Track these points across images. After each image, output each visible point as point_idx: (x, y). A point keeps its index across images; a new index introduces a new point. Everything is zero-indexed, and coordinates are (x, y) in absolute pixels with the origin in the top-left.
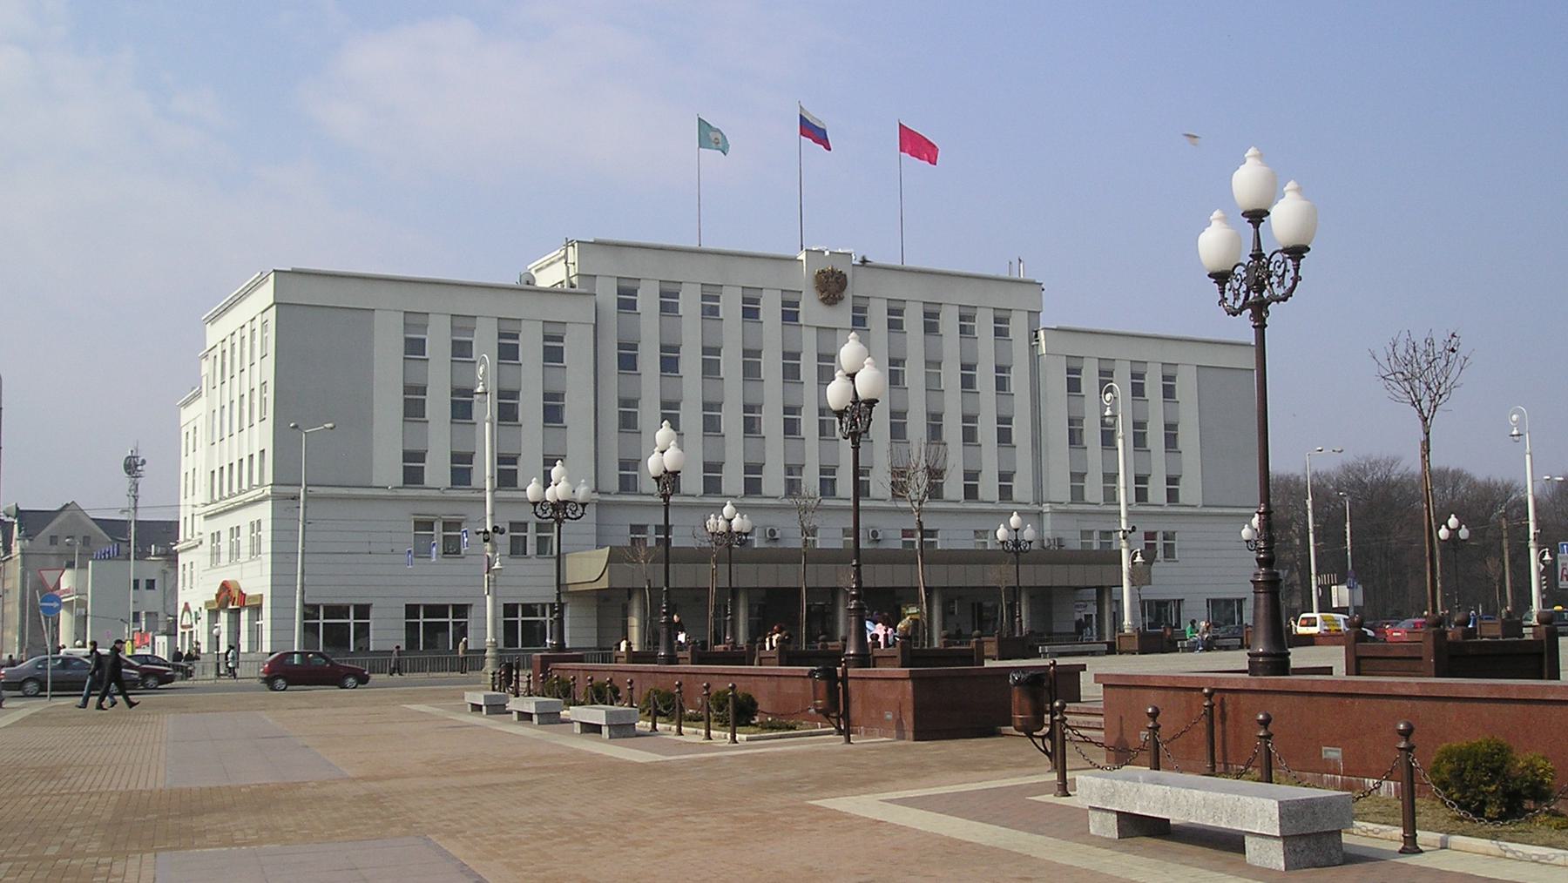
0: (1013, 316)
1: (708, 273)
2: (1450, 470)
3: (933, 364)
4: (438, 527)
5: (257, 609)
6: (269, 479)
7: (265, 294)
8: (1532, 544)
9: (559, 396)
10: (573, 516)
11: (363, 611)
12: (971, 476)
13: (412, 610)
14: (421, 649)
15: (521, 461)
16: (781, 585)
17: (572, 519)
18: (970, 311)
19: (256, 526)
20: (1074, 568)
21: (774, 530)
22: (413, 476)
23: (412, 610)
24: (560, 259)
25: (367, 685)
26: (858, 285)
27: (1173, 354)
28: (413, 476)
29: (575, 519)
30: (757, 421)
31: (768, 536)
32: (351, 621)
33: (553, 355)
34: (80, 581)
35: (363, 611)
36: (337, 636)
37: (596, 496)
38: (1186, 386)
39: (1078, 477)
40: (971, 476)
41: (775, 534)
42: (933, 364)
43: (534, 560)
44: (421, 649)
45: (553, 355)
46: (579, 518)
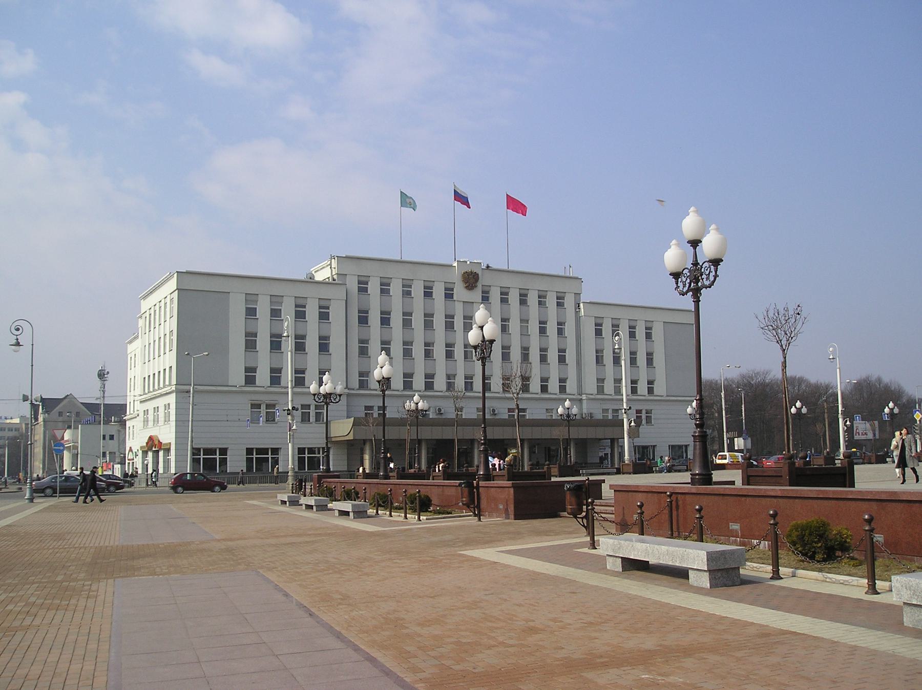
2: (797, 377)
3: (524, 321)
4: (263, 407)
5: (168, 450)
6: (174, 382)
7: (172, 284)
8: (840, 416)
9: (327, 338)
10: (335, 401)
13: (249, 451)
14: (254, 471)
17: (334, 403)
19: (167, 406)
22: (250, 380)
23: (249, 451)
24: (327, 266)
26: (484, 280)
27: (650, 316)
28: (250, 380)
29: (336, 403)
32: (218, 457)
33: (324, 316)
34: (75, 436)
37: (347, 391)
38: (658, 333)
40: (544, 380)
42: (524, 321)
43: (314, 425)
44: (254, 471)
45: (324, 316)
46: (338, 402)
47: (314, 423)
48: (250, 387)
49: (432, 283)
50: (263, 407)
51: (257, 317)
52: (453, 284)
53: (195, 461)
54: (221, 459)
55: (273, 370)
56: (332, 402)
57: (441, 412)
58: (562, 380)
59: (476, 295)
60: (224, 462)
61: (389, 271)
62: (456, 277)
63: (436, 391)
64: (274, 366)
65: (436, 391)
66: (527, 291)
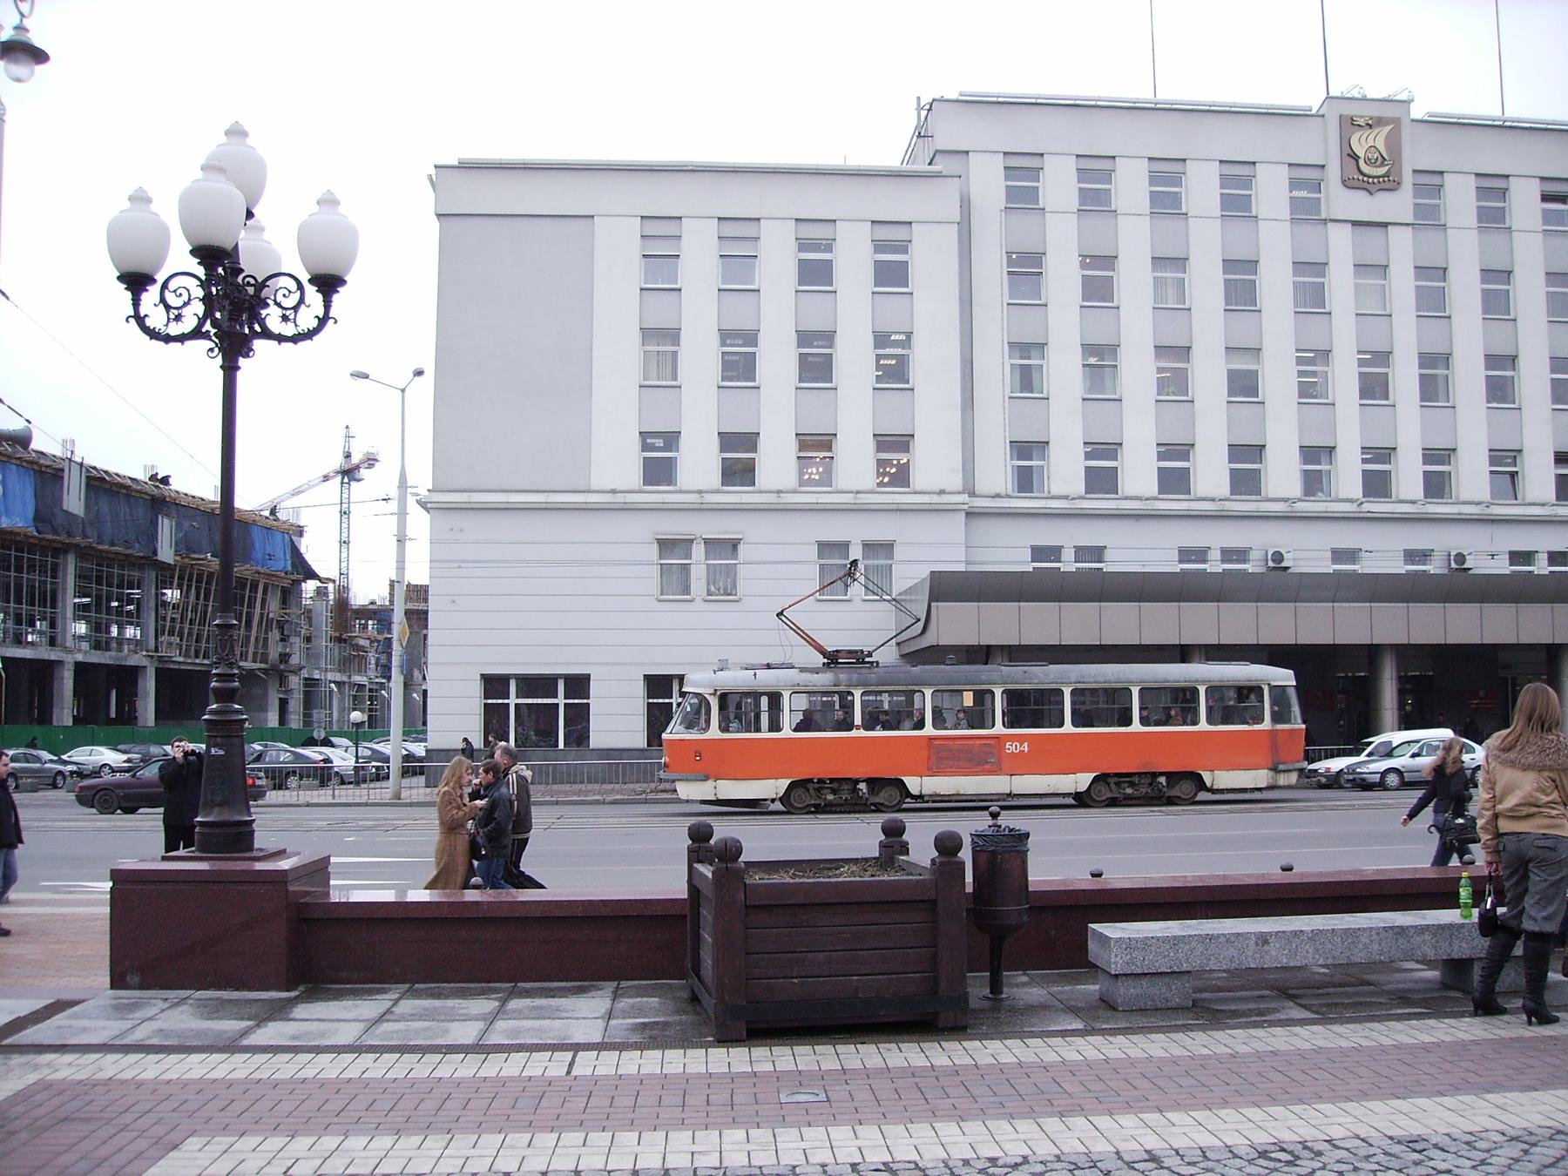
0: (1118, 168)
1: (1163, 140)
3: (1170, 263)
4: (698, 550)
10: (289, 330)
11: (578, 685)
12: (1175, 451)
13: (494, 685)
14: (561, 745)
15: (918, 444)
16: (1449, 641)
17: (281, 338)
18: (1244, 171)
20: (1491, 609)
21: (1464, 556)
22: (659, 471)
23: (494, 685)
25: (260, 802)
26: (1417, 156)
27: (816, 199)
28: (659, 471)
30: (1441, 382)
31: (1454, 565)
32: (561, 700)
33: (891, 275)
35: (578, 685)
36: (539, 726)
39: (1027, 450)
40: (1175, 451)
41: (1282, 560)
42: (1170, 263)
43: (698, 604)
44: (561, 745)
45: (891, 275)
47: (698, 600)
48: (1405, 513)
49: (1177, 167)
50: (698, 550)
51: (1326, 310)
52: (1320, 170)
53: (494, 720)
54: (525, 711)
55: (729, 441)
56: (267, 334)
57: (1284, 564)
58: (893, 443)
59: (1397, 205)
60: (579, 718)
61: (1103, 137)
62: (1321, 147)
63: (1127, 498)
64: (1311, 442)
65: (1127, 498)
66: (1110, 161)
